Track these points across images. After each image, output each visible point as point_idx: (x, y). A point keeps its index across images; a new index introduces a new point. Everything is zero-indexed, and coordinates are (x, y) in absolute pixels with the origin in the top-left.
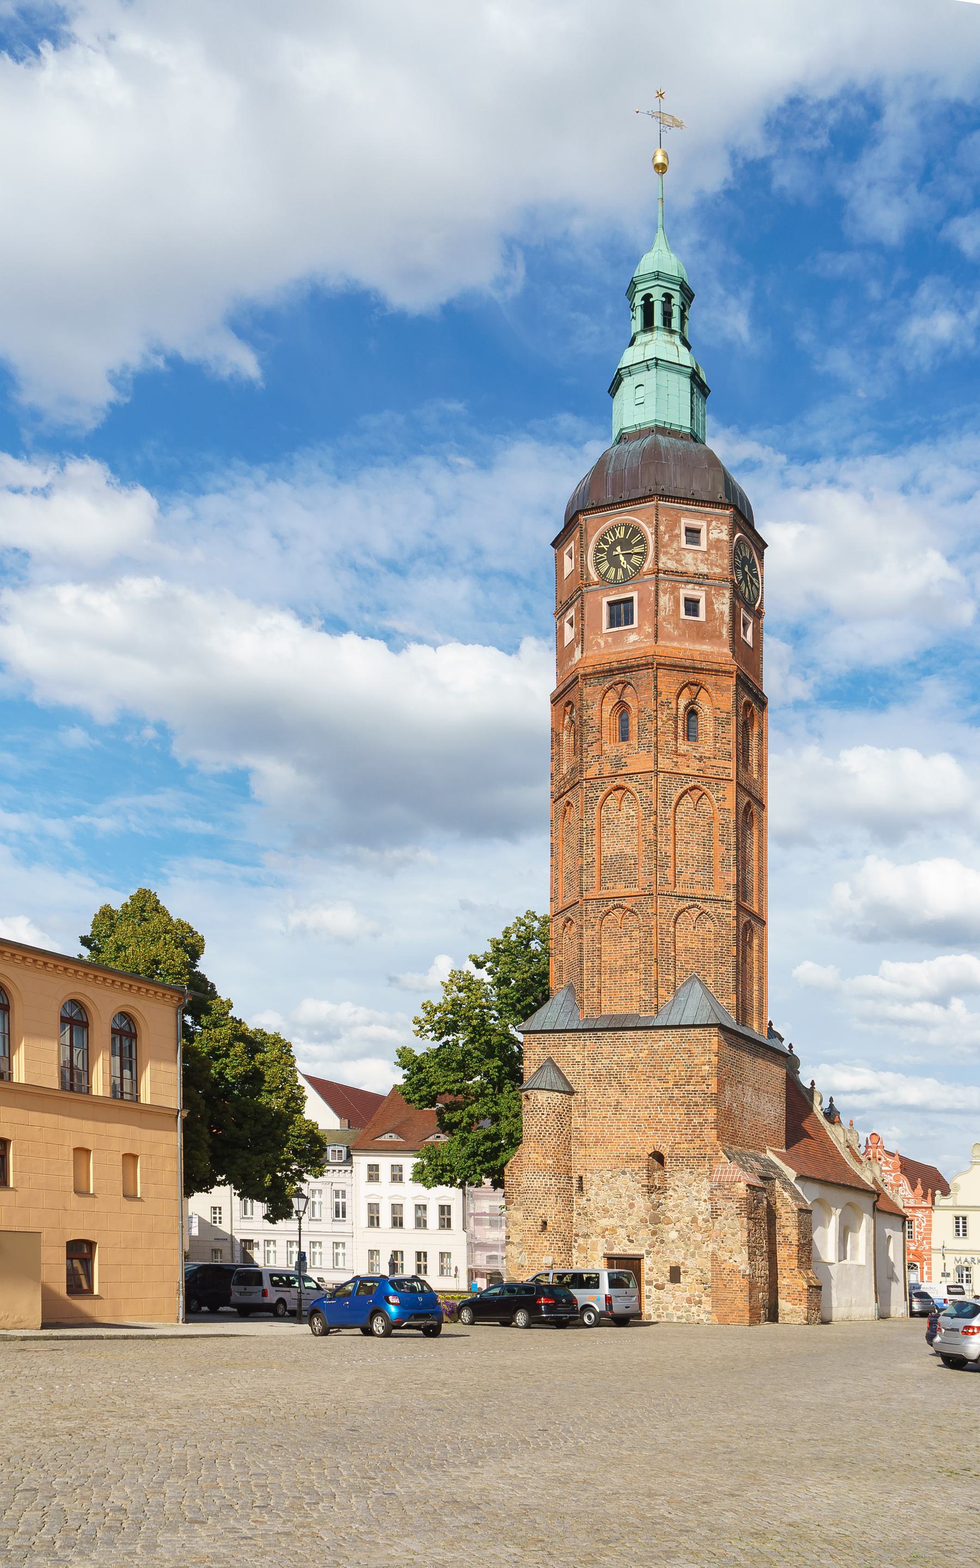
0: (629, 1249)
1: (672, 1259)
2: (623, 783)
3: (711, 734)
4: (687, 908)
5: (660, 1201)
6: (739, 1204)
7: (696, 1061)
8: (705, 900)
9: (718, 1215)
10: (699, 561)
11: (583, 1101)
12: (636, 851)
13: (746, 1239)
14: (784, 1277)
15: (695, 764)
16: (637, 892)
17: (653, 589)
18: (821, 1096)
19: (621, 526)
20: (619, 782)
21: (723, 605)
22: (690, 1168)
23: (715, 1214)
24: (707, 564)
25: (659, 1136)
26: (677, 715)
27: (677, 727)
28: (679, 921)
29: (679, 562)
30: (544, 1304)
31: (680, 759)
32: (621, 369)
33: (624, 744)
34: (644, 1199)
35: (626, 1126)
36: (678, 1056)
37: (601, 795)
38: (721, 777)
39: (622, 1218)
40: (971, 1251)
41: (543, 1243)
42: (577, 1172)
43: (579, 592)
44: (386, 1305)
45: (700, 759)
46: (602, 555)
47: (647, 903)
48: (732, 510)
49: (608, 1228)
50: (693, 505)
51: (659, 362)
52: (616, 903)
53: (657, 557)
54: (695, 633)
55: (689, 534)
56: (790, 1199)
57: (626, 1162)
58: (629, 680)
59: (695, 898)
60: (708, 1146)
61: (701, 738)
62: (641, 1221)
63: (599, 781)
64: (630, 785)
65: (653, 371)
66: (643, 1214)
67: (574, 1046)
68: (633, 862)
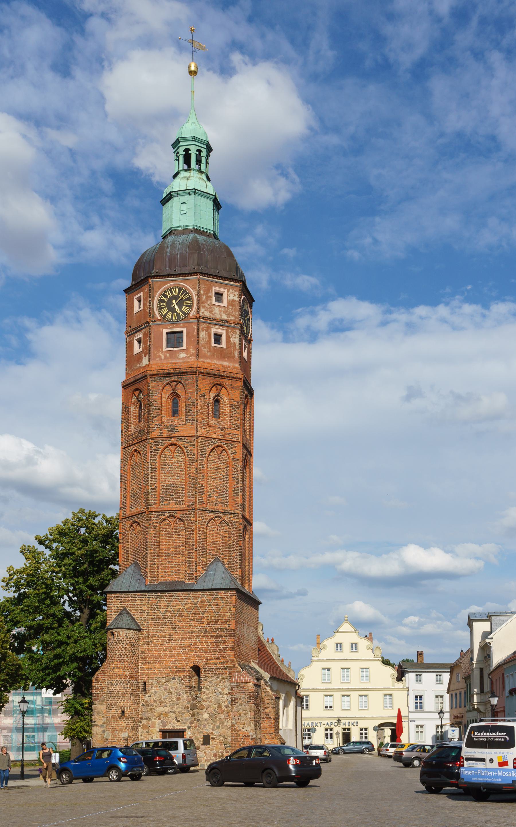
0: (176, 726)
1: (204, 731)
2: (175, 442)
3: (228, 414)
4: (214, 518)
5: (198, 696)
6: (249, 695)
7: (222, 610)
8: (224, 513)
9: (236, 703)
10: (222, 313)
11: (147, 635)
12: (183, 483)
13: (253, 717)
14: (266, 739)
15: (219, 432)
16: (184, 508)
17: (196, 327)
18: (262, 625)
19: (176, 288)
20: (173, 441)
21: (235, 339)
22: (217, 675)
23: (233, 702)
24: (227, 314)
25: (197, 656)
26: (209, 402)
27: (209, 410)
28: (209, 525)
29: (211, 312)
30: (158, 761)
31: (211, 429)
32: (172, 192)
33: (175, 419)
34: (187, 695)
35: (176, 650)
36: (210, 607)
37: (161, 448)
38: (234, 440)
39: (172, 707)
40: (311, 718)
41: (121, 724)
42: (142, 679)
43: (147, 324)
44: (119, 763)
45: (222, 429)
46: (164, 304)
47: (190, 515)
48: (241, 283)
49: (163, 713)
50: (219, 279)
51: (197, 191)
52: (170, 514)
53: (198, 309)
54: (220, 355)
55: (217, 295)
56: (270, 692)
57: (175, 672)
58: (180, 380)
59: (219, 512)
60: (228, 661)
61: (222, 416)
62: (185, 708)
63: (160, 439)
64: (180, 443)
65: (193, 196)
66: (186, 704)
67: (142, 601)
68: (181, 489)
